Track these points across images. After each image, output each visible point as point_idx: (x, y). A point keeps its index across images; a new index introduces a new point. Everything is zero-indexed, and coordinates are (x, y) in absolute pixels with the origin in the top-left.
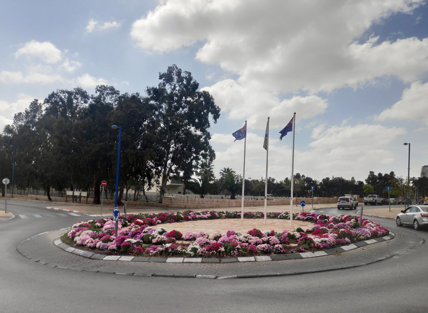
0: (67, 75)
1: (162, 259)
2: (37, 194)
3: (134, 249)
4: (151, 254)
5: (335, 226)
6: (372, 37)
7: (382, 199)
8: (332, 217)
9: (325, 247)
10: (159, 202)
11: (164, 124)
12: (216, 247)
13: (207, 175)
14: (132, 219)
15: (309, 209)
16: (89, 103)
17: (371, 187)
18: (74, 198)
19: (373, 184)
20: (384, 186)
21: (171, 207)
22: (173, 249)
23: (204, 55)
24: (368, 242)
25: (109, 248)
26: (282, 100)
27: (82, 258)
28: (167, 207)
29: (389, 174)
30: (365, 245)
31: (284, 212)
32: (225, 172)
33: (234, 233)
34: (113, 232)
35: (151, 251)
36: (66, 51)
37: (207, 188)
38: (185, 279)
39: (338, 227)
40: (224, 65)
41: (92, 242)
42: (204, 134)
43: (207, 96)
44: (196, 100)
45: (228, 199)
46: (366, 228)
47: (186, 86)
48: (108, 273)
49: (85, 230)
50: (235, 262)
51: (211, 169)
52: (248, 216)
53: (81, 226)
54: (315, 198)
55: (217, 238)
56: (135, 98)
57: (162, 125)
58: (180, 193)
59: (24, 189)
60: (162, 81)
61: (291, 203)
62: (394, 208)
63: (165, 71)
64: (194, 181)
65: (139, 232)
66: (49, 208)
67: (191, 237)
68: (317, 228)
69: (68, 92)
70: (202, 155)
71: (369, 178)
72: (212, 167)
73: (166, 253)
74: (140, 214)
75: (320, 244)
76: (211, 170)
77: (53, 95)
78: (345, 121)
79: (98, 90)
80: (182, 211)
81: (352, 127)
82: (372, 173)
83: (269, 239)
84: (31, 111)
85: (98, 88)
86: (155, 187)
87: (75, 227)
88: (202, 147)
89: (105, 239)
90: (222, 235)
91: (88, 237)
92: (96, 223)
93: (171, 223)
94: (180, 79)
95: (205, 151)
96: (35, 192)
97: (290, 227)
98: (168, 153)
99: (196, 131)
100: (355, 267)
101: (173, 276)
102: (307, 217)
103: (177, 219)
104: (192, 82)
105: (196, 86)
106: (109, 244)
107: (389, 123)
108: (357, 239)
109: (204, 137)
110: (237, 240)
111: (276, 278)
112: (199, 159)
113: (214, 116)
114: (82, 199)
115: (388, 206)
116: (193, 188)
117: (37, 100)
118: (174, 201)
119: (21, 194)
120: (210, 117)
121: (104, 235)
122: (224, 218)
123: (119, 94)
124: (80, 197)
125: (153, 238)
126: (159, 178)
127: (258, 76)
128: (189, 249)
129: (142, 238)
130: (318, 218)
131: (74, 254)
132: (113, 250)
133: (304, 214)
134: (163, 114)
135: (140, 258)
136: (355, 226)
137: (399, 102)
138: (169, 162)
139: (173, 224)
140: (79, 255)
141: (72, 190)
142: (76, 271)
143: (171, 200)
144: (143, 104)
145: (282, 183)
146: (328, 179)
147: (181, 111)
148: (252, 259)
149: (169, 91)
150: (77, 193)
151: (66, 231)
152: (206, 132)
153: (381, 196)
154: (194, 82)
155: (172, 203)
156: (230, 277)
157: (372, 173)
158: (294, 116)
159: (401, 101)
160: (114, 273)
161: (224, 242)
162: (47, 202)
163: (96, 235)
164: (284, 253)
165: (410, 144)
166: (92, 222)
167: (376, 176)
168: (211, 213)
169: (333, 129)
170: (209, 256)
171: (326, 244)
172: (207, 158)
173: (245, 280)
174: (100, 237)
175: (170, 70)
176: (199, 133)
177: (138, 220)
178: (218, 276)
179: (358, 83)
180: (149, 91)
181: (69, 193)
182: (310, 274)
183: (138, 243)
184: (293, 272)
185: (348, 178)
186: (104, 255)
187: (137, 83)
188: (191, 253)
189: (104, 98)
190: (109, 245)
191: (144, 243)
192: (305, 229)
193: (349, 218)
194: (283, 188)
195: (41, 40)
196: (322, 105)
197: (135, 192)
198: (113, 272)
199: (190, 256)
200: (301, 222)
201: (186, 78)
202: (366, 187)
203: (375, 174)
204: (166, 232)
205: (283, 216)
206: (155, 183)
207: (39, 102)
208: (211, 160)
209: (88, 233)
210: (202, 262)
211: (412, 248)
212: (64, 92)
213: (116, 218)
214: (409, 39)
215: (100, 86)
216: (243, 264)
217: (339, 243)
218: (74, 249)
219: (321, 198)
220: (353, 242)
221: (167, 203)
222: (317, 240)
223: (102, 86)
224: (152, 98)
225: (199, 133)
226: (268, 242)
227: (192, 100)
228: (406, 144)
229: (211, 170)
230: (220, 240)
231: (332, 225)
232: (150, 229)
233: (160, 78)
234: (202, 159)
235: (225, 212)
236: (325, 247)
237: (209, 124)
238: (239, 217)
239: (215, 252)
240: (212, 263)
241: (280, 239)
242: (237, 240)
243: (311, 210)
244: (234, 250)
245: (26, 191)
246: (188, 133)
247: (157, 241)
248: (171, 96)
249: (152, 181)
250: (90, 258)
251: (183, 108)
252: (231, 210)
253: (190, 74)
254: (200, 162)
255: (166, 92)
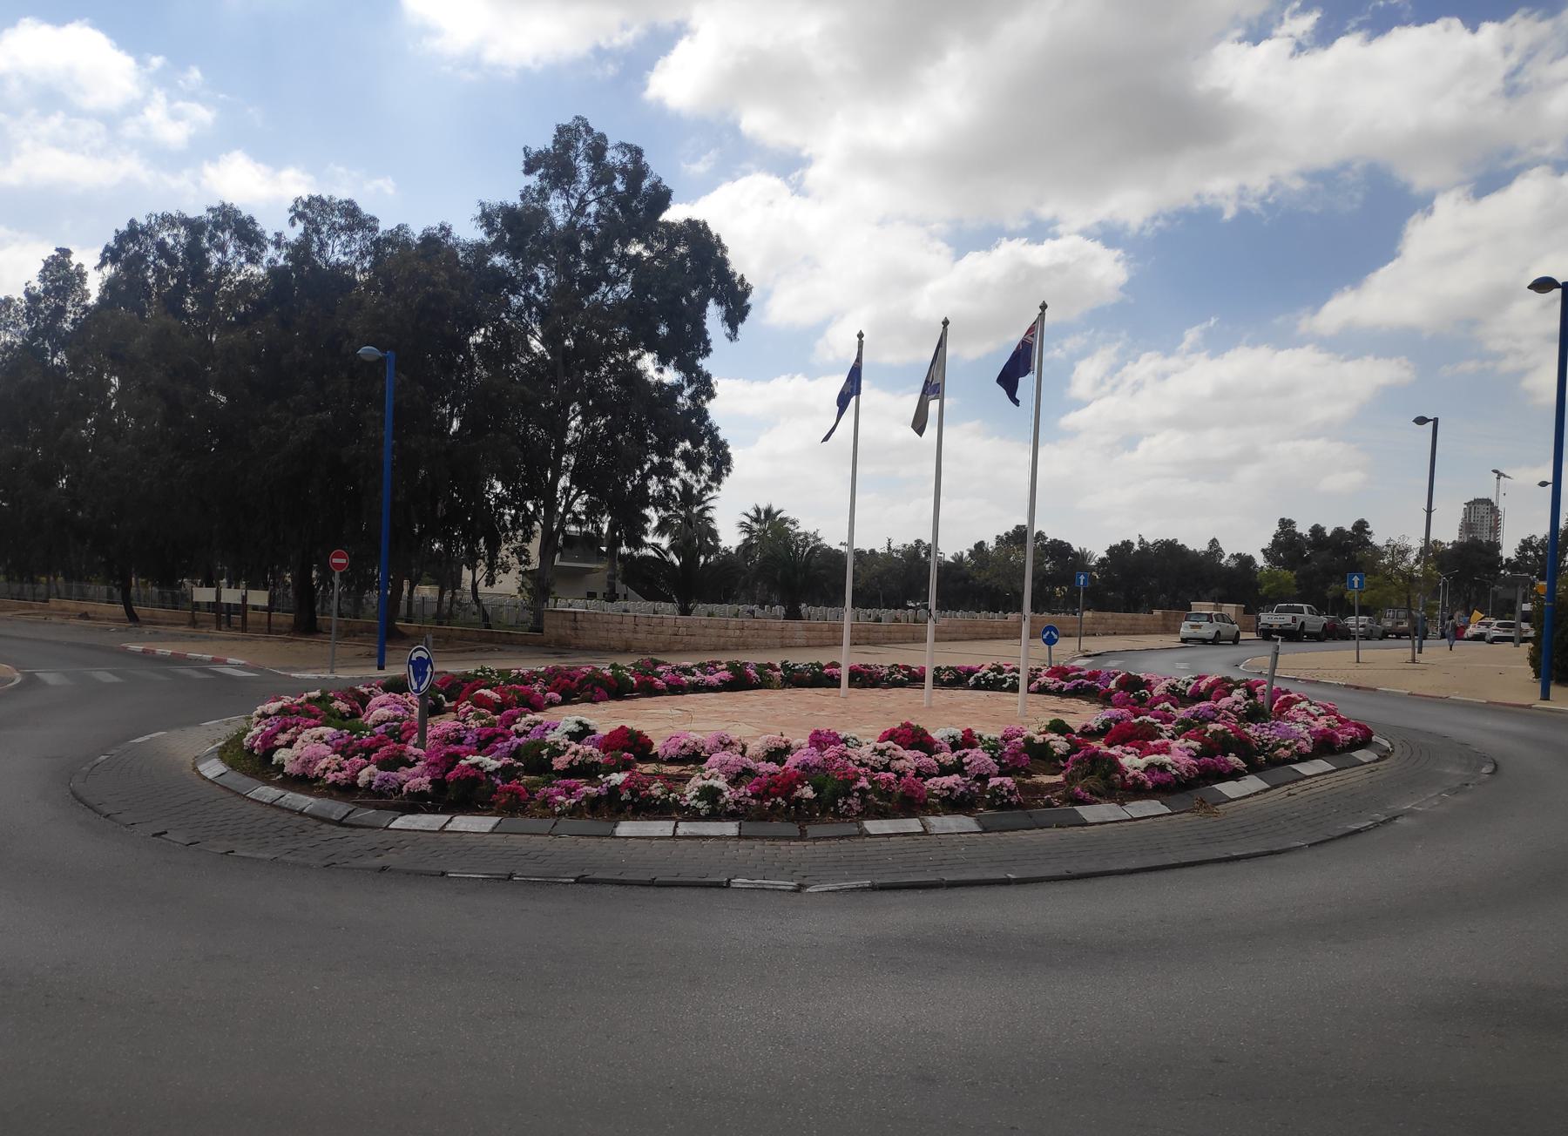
0: (162, 157)
1: (600, 826)
2: (83, 597)
3: (495, 792)
4: (558, 809)
5: (1181, 713)
6: (1294, 14)
7: (1324, 619)
8: (1165, 684)
9: (1165, 786)
10: (533, 632)
11: (542, 342)
12: (786, 786)
13: (693, 530)
14: (458, 688)
15: (1067, 651)
16: (265, 261)
17: (1288, 575)
18: (222, 615)
19: (1289, 564)
20: (1342, 574)
21: (578, 648)
22: (634, 793)
23: (678, 83)
24: (1305, 768)
25: (405, 789)
26: (959, 256)
27: (313, 822)
28: (561, 647)
29: (1348, 528)
30: (1296, 781)
31: (989, 665)
32: (756, 520)
33: (835, 740)
34: (407, 734)
35: (560, 798)
36: (157, 61)
37: (699, 577)
38: (695, 892)
39: (1194, 717)
40: (757, 121)
41: (341, 770)
42: (690, 383)
43: (699, 238)
44: (659, 254)
45: (776, 617)
46: (1293, 719)
47: (623, 201)
48: (420, 874)
49: (310, 727)
50: (854, 836)
51: (707, 508)
52: (863, 678)
53: (282, 711)
54: (1087, 614)
55: (777, 754)
56: (435, 244)
57: (536, 345)
58: (592, 596)
59: (32, 581)
60: (533, 180)
61: (930, 635)
62: (1374, 653)
63: (543, 141)
64: (652, 553)
65: (502, 735)
66: (137, 647)
67: (684, 752)
68: (1117, 722)
69: (187, 222)
70: (685, 456)
71: (1275, 543)
72: (710, 503)
73: (612, 806)
74: (483, 670)
75: (1143, 776)
76: (708, 514)
77: (133, 233)
78: (1192, 335)
79: (301, 216)
80: (626, 661)
81: (1212, 357)
82: (1286, 524)
83: (960, 758)
84: (46, 291)
85: (300, 208)
86: (513, 573)
87: (265, 716)
88: (682, 431)
89: (386, 759)
90: (794, 743)
91: (324, 749)
92: (333, 700)
93: (594, 702)
94: (603, 175)
95: (695, 445)
96: (75, 590)
97: (1028, 715)
98: (563, 449)
99: (661, 371)
100: (1272, 853)
101: (652, 884)
102: (1073, 683)
103: (616, 690)
104: (646, 184)
105: (662, 198)
106: (403, 774)
107: (1351, 344)
108: (1268, 759)
109: (688, 392)
110: (850, 763)
111: (1003, 889)
112: (674, 474)
113: (728, 311)
114: (251, 615)
115: (1353, 643)
116: (648, 579)
117: (66, 253)
118: (585, 625)
119: (20, 596)
120: (714, 315)
121: (380, 743)
122: (779, 688)
123: (376, 229)
124: (242, 608)
125: (556, 752)
126: (527, 539)
127: (877, 163)
128: (690, 791)
129: (515, 754)
130: (1112, 685)
131: (279, 807)
132: (422, 795)
133: (1060, 672)
134: (539, 305)
135: (520, 822)
136: (1254, 714)
137: (1391, 265)
138: (564, 482)
139: (601, 705)
140: (301, 813)
141: (209, 582)
142: (307, 866)
143: (575, 620)
144: (467, 266)
145: (959, 559)
146: (1127, 545)
147: (605, 295)
148: (913, 825)
149: (560, 220)
150: (231, 596)
151: (231, 730)
152: (699, 373)
153: (1320, 607)
154: (655, 186)
155: (580, 633)
156: (846, 885)
157: (1286, 524)
158: (1042, 315)
159: (1397, 261)
160: (443, 874)
161: (805, 767)
162: (124, 626)
163: (350, 743)
164: (1019, 805)
165: (1436, 421)
166: (319, 700)
167: (1300, 535)
168: (732, 667)
169: (1147, 365)
170: (764, 817)
171: (1164, 777)
172: (702, 472)
173: (901, 896)
174: (368, 751)
175: (566, 136)
176: (671, 376)
177: (482, 691)
178: (806, 881)
179: (1243, 188)
180: (487, 218)
181: (204, 595)
182: (1121, 879)
183: (506, 772)
184: (1061, 871)
185: (1196, 543)
186: (391, 814)
187: (442, 192)
188: (700, 805)
189: (323, 246)
190: (404, 777)
191: (528, 770)
192: (1075, 722)
193: (1223, 687)
194: (966, 578)
195: (58, 17)
196: (1108, 270)
197: (441, 594)
198: (435, 867)
199: (695, 816)
200: (1054, 698)
201: (624, 171)
202: (1271, 576)
203: (1298, 530)
204: (594, 732)
205: (987, 680)
206: (513, 560)
207: (75, 259)
208: (717, 477)
209: (321, 737)
210: (740, 836)
211: (1455, 791)
212: (169, 221)
213: (419, 685)
214: (1432, 26)
215: (306, 199)
216: (885, 843)
217: (1207, 774)
218: (279, 792)
219: (1108, 615)
220: (1254, 768)
221: (562, 632)
222: (1132, 762)
223: (311, 198)
224: (497, 247)
225: (671, 376)
226: (958, 768)
227: (646, 254)
228: (1421, 421)
229: (708, 514)
230: (792, 761)
231: (1167, 710)
232: (537, 723)
233: (529, 170)
234: (682, 474)
235: (778, 665)
236: (1165, 786)
237: (707, 343)
238: (833, 682)
239: (784, 803)
240: (774, 838)
241: (1000, 757)
242: (850, 763)
243: (1074, 659)
244: (849, 795)
245: (42, 588)
246: (633, 378)
247: (570, 763)
248: (569, 238)
249: (504, 551)
250: (340, 823)
251: (613, 281)
252: (802, 659)
253: (638, 152)
254: (675, 482)
255: (551, 223)
